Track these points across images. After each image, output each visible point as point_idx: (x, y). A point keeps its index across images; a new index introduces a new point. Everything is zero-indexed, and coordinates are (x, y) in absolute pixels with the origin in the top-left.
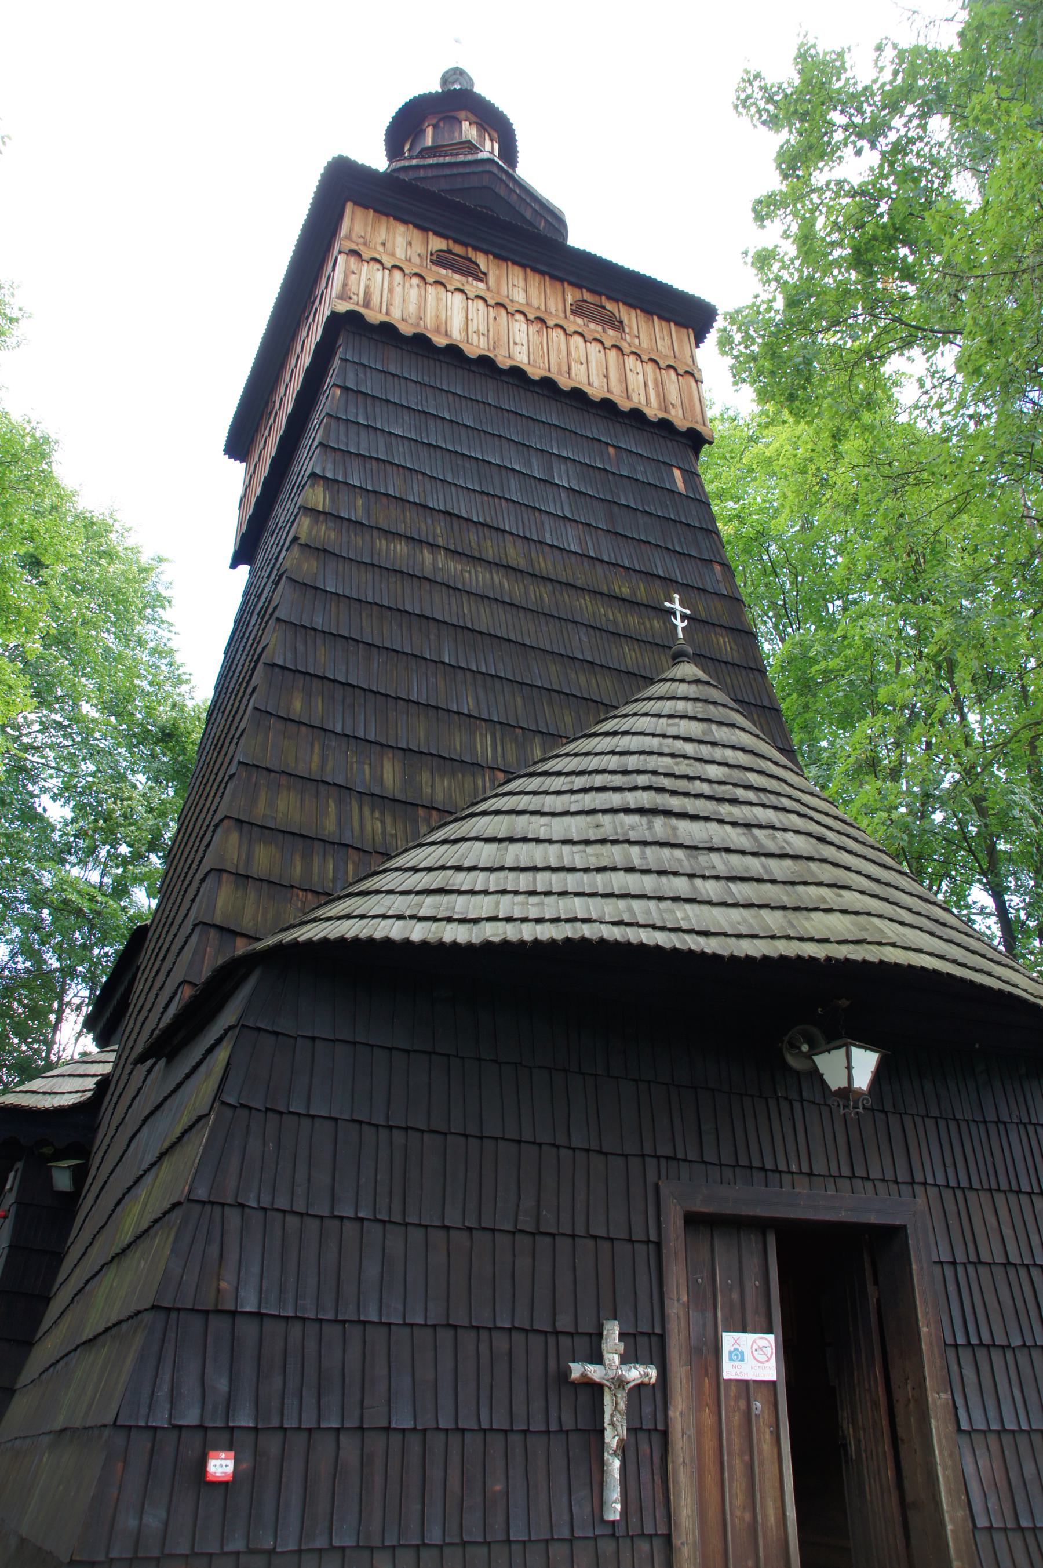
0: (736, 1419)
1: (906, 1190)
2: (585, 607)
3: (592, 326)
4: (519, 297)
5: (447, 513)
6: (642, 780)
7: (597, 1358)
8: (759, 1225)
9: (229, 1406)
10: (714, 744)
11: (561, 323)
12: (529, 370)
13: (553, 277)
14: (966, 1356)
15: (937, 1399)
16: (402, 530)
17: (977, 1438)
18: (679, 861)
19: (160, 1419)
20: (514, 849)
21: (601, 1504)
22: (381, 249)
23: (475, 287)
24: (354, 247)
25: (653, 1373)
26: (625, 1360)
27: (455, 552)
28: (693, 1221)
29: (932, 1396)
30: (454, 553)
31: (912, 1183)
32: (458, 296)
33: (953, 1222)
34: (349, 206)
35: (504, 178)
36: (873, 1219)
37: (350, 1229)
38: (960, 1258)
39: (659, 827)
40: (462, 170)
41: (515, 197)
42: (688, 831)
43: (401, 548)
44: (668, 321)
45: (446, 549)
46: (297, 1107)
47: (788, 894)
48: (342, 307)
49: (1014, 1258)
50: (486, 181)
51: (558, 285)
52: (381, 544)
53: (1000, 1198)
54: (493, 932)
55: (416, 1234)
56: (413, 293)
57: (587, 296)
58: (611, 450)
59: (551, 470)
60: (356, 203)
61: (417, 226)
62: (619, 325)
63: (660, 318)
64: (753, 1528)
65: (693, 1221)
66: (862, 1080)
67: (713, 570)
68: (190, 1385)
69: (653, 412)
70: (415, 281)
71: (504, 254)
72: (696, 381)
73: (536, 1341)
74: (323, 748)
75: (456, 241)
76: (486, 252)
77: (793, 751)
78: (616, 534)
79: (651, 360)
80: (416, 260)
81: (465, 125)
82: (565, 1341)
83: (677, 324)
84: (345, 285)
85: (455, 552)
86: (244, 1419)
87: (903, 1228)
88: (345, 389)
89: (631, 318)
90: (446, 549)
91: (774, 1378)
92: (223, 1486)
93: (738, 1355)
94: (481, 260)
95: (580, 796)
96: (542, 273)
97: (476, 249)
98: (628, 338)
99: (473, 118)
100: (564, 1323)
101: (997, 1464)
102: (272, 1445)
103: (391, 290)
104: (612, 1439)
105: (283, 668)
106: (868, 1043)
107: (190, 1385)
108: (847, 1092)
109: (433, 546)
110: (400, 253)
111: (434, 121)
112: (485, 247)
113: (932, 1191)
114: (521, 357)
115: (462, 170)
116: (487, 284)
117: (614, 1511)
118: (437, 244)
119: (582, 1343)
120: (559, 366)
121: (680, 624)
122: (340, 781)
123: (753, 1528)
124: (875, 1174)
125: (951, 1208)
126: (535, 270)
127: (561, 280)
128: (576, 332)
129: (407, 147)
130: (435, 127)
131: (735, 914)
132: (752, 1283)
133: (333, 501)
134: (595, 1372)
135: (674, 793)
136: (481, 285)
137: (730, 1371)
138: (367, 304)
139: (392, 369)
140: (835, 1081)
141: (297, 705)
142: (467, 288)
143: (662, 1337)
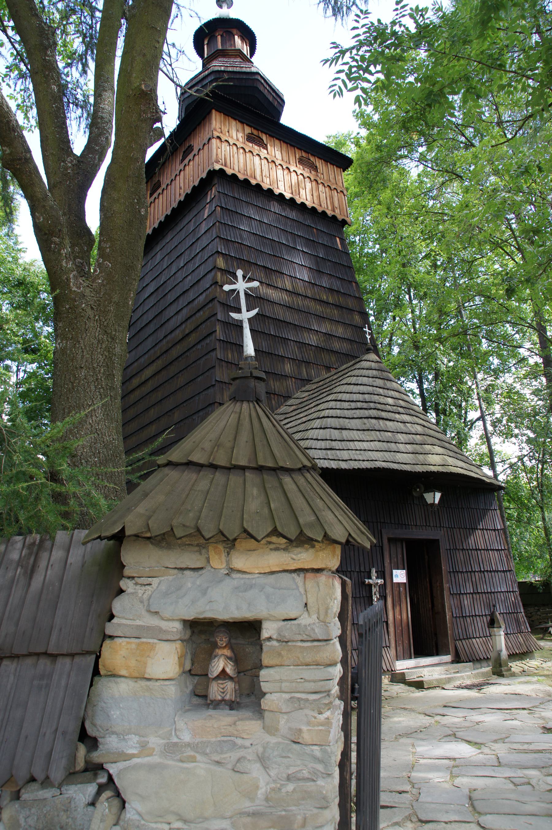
0: (397, 593)
1: (439, 529)
5: (264, 267)
6: (372, 405)
7: (370, 577)
8: (401, 540)
13: (291, 145)
14: (452, 575)
15: (446, 586)
17: (454, 596)
18: (389, 436)
22: (227, 134)
23: (263, 153)
24: (218, 135)
27: (268, 285)
28: (390, 540)
29: (444, 585)
31: (440, 527)
33: (450, 537)
34: (214, 111)
35: (263, 81)
36: (431, 538)
38: (452, 548)
44: (333, 165)
47: (421, 448)
48: (217, 167)
49: (465, 548)
51: (293, 148)
53: (461, 530)
56: (241, 157)
57: (304, 154)
58: (315, 230)
60: (216, 110)
61: (240, 121)
62: (315, 169)
63: (331, 164)
65: (390, 540)
66: (437, 501)
67: (352, 285)
69: (330, 213)
71: (273, 135)
75: (255, 128)
76: (266, 134)
78: (320, 271)
79: (328, 186)
80: (241, 139)
81: (236, 37)
82: (362, 574)
83: (337, 166)
84: (217, 155)
85: (268, 285)
87: (438, 540)
88: (222, 208)
89: (319, 163)
91: (405, 581)
93: (397, 576)
94: (264, 137)
95: (355, 411)
96: (287, 143)
97: (262, 132)
98: (319, 175)
99: (239, 33)
101: (459, 602)
103: (233, 157)
105: (223, 341)
106: (439, 491)
108: (433, 504)
111: (221, 33)
112: (266, 131)
113: (445, 529)
116: (267, 150)
118: (248, 130)
119: (366, 574)
120: (295, 191)
124: (432, 525)
125: (449, 534)
126: (284, 142)
127: (294, 146)
129: (206, 42)
130: (222, 36)
132: (400, 556)
134: (371, 581)
137: (395, 580)
138: (225, 166)
139: (236, 196)
142: (261, 154)
143: (384, 572)
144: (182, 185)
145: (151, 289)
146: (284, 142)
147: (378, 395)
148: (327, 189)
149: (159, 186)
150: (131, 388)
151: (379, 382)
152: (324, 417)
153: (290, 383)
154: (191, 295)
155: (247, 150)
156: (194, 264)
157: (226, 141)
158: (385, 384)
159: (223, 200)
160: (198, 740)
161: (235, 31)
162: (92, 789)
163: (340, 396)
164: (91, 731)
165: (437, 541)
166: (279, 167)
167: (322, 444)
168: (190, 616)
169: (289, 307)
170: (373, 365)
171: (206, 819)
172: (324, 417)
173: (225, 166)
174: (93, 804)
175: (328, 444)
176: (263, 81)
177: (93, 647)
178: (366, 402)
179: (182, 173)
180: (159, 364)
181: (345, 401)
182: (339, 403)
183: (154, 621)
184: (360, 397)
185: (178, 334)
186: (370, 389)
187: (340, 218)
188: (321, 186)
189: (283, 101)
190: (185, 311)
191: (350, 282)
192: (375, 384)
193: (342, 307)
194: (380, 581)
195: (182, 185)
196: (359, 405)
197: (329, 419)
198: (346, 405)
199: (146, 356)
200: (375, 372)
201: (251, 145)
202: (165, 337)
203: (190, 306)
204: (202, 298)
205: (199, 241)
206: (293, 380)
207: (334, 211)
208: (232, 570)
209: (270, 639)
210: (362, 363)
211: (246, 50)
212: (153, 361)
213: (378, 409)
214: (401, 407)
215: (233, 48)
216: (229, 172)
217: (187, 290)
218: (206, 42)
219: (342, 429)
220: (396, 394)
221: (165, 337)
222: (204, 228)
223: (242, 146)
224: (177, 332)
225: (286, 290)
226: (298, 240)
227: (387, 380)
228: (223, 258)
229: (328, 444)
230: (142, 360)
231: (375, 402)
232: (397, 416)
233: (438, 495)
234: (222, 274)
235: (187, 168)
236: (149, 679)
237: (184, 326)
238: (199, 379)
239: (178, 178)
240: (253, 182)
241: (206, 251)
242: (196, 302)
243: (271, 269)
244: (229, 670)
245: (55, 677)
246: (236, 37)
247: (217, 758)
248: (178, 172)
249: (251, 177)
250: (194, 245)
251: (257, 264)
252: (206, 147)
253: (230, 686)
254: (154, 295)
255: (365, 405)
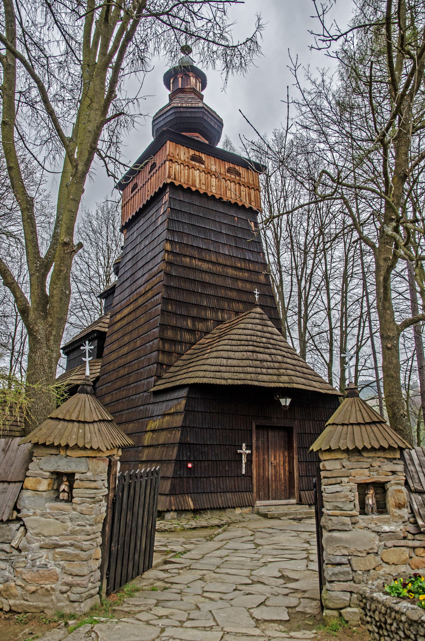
2: (230, 271)
3: (232, 176)
4: (213, 168)
5: (197, 247)
6: (251, 343)
7: (242, 450)
9: (190, 457)
10: (264, 332)
11: (224, 177)
12: (216, 195)
16: (188, 254)
19: (181, 459)
20: (230, 361)
21: (241, 471)
22: (177, 157)
24: (171, 158)
25: (250, 451)
26: (246, 450)
28: (257, 427)
29: (295, 456)
30: (199, 259)
32: (198, 171)
34: (168, 141)
37: (205, 430)
39: (255, 356)
40: (194, 110)
41: (209, 119)
42: (261, 356)
43: (188, 259)
45: (198, 258)
46: (196, 410)
50: (201, 115)
52: (183, 259)
54: (230, 382)
55: (214, 430)
58: (236, 218)
59: (221, 229)
60: (170, 141)
64: (264, 476)
66: (288, 404)
68: (185, 455)
70: (187, 167)
72: (259, 192)
73: (232, 447)
74: (176, 318)
76: (205, 154)
77: (279, 319)
86: (192, 459)
88: (171, 208)
90: (198, 258)
92: (190, 468)
94: (203, 156)
97: (202, 153)
99: (194, 75)
100: (237, 444)
102: (196, 463)
104: (243, 462)
105: (166, 298)
106: (290, 397)
107: (185, 455)
108: (285, 406)
109: (195, 258)
110: (182, 158)
111: (181, 76)
114: (214, 191)
115: (194, 110)
117: (244, 472)
118: (192, 152)
121: (257, 297)
122: (180, 326)
123: (264, 476)
128: (228, 180)
129: (171, 81)
130: (182, 78)
131: (269, 377)
133: (172, 247)
135: (257, 347)
136: (203, 166)
140: (283, 404)
141: (170, 307)
144: (149, 189)
145: (130, 256)
146: (217, 158)
147: (256, 336)
148: (247, 189)
149: (137, 187)
150: (116, 320)
151: (259, 327)
152: (219, 351)
153: (210, 324)
154: (150, 266)
155: (190, 167)
156: (154, 244)
157: (176, 162)
158: (263, 328)
159: (172, 203)
160: (51, 511)
161: (191, 74)
162: (18, 525)
163: (232, 337)
164: (19, 507)
165: (292, 428)
166: (213, 176)
167: (213, 368)
168: (52, 470)
169: (213, 273)
170: (257, 316)
171: (51, 536)
172: (219, 351)
173: (175, 179)
174: (18, 530)
175: (217, 368)
176: (207, 113)
177: (21, 479)
178: (247, 341)
179: (149, 181)
180: (131, 307)
181: (234, 340)
182: (230, 341)
183: (41, 472)
184: (244, 337)
185: (142, 290)
186: (252, 332)
187: (255, 208)
188: (242, 187)
189: (223, 125)
190: (146, 275)
191: (259, 253)
192: (256, 329)
193: (251, 271)
194: (248, 452)
195: (149, 189)
196: (243, 342)
197: (223, 352)
198: (234, 342)
199: (125, 301)
200: (258, 321)
201: (229, 175)
202: (136, 290)
203: (150, 272)
204: (156, 268)
205: (157, 230)
206: (212, 321)
207: (251, 204)
208: (67, 456)
209: (77, 479)
210: (251, 314)
211: (199, 86)
212: (128, 305)
213: (254, 346)
214: (270, 344)
215: (189, 87)
216: (177, 183)
217: (149, 261)
218: (171, 81)
219: (228, 359)
220: (269, 335)
221: (136, 290)
222: (160, 221)
223: (187, 164)
224: (142, 288)
225: (212, 262)
226: (223, 226)
227: (265, 326)
228: (170, 243)
229: (217, 368)
230: (123, 303)
231: (253, 341)
232: (267, 350)
233: (289, 401)
234: (168, 254)
235: (152, 178)
236: (38, 491)
237: (146, 284)
238: (151, 321)
239: (144, 186)
240: (194, 189)
241: (160, 237)
242: (153, 270)
243: (202, 248)
244: (66, 489)
245: (9, 489)
246: (192, 78)
247: (56, 517)
248: (147, 180)
249: (193, 185)
250: (154, 232)
251: (192, 246)
252: (163, 166)
253: (66, 494)
254: (131, 261)
255: (246, 343)
